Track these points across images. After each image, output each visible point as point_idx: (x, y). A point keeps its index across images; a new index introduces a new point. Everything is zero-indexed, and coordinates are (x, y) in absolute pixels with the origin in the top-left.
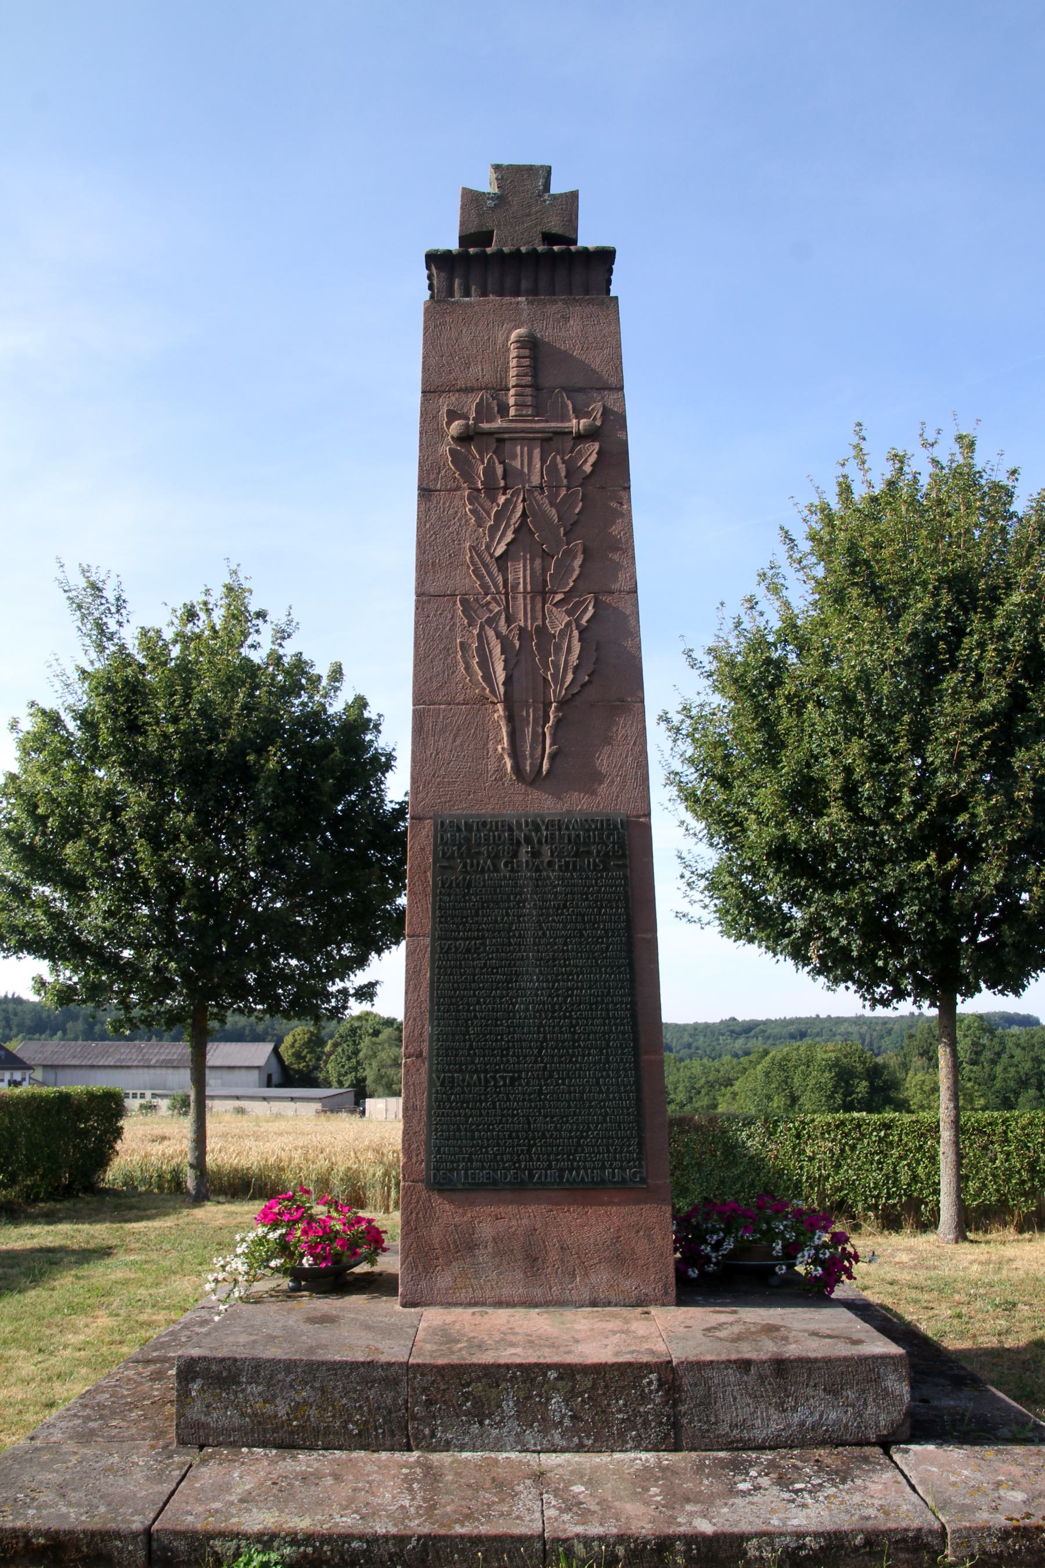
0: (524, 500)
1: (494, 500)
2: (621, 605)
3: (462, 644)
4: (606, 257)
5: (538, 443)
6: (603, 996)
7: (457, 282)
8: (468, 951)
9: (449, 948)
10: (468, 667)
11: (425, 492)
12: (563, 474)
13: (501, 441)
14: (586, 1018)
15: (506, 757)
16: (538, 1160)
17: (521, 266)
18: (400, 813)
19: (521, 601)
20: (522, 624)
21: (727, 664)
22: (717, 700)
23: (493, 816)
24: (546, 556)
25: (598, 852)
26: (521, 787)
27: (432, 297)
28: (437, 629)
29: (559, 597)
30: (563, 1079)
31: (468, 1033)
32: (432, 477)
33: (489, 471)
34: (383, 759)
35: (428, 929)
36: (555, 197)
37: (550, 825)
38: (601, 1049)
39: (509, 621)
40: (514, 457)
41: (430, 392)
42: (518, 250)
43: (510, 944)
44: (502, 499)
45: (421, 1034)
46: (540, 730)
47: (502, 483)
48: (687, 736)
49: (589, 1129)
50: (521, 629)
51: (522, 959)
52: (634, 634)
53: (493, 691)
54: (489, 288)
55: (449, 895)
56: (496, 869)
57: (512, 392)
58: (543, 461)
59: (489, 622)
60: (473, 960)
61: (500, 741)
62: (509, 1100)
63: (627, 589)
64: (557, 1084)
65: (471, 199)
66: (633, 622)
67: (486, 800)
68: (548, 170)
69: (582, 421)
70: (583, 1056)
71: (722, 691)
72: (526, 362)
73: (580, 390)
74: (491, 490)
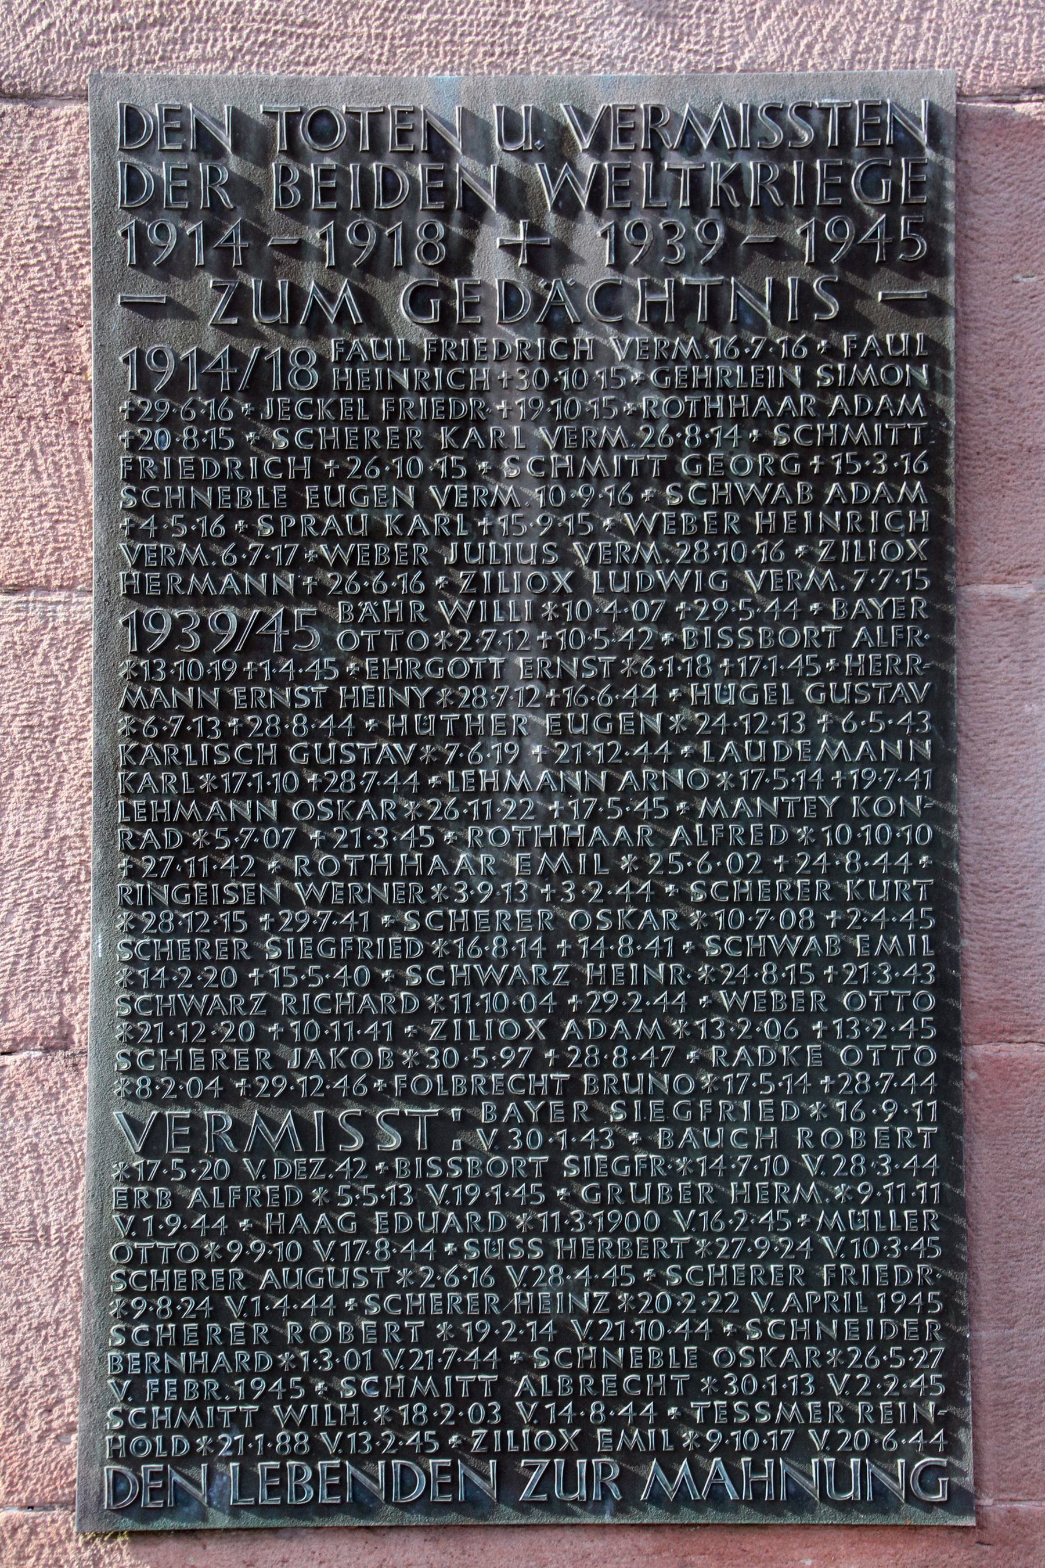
6: (820, 818)
8: (256, 645)
9: (176, 636)
14: (748, 906)
15: (459, 150)
16: (540, 1418)
23: (357, 89)
25: (824, 249)
30: (646, 1127)
31: (257, 958)
35: (85, 563)
37: (610, 130)
38: (805, 1019)
43: (435, 622)
45: (64, 966)
49: (746, 1309)
51: (486, 678)
55: (171, 421)
56: (374, 318)
60: (278, 681)
62: (423, 1202)
64: (621, 1145)
70: (731, 1043)
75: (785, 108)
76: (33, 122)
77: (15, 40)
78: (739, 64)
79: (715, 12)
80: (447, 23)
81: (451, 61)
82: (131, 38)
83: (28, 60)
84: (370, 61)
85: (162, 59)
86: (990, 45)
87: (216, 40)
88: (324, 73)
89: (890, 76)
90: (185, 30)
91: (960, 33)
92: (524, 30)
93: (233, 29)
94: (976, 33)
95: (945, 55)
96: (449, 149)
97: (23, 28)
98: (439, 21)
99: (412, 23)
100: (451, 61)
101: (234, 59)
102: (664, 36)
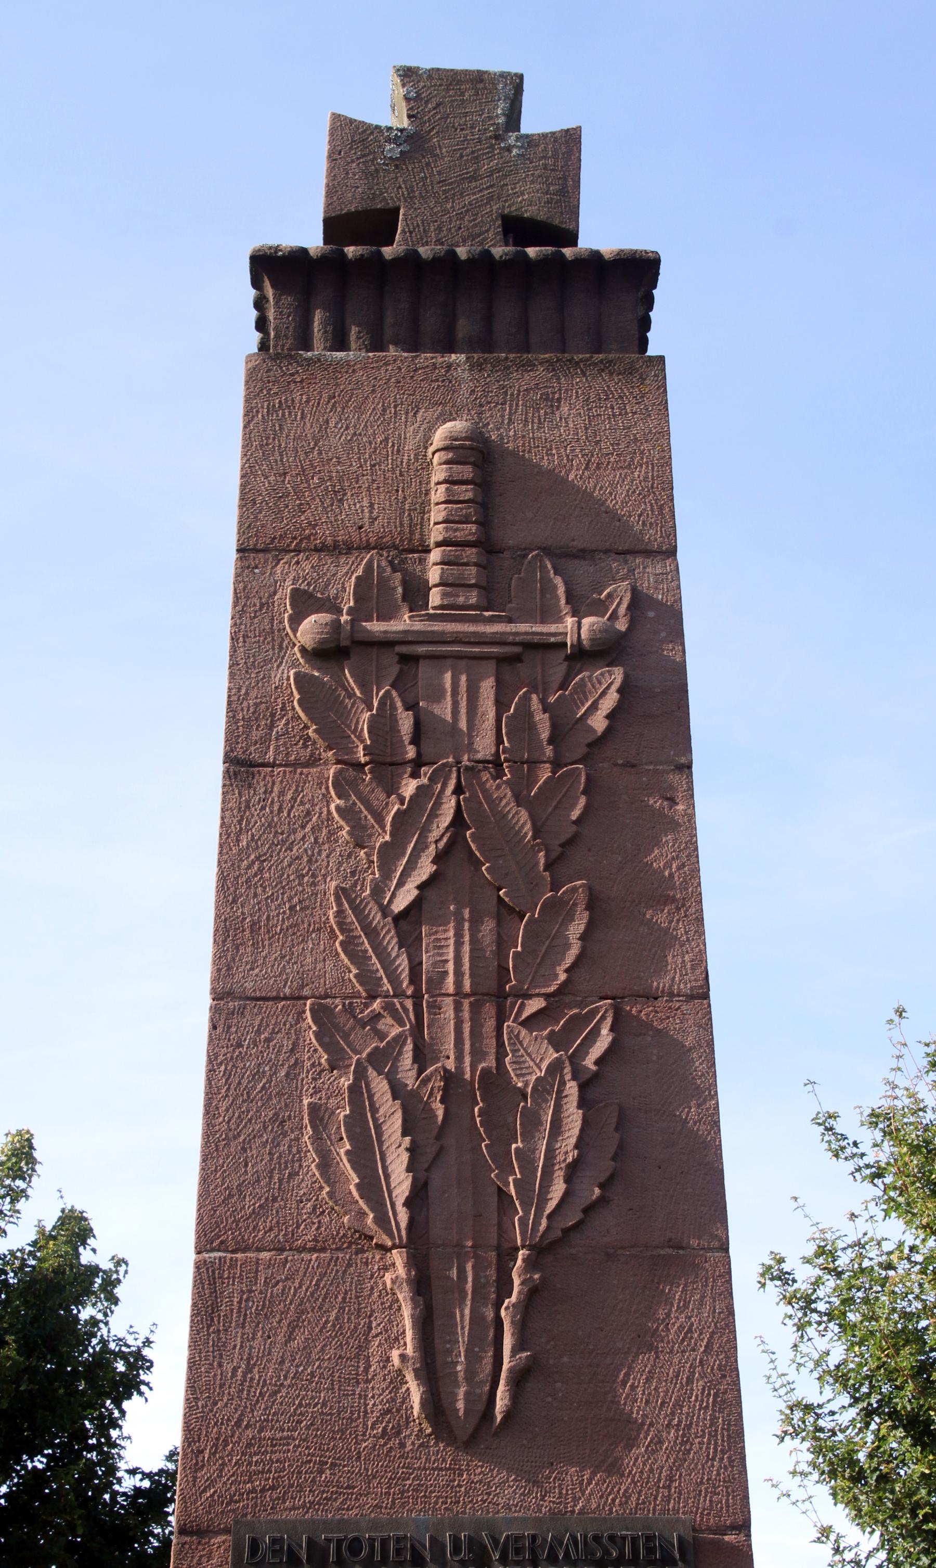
0: (458, 790)
1: (392, 789)
2: (673, 1025)
3: (313, 1108)
4: (639, 271)
5: (491, 666)
7: (318, 317)
10: (326, 1164)
11: (240, 768)
12: (545, 735)
13: (408, 660)
15: (410, 1377)
17: (453, 278)
18: (154, 1497)
19: (449, 1012)
20: (451, 1065)
21: (914, 1150)
22: (895, 1231)
23: (375, 1525)
24: (506, 913)
26: (442, 1453)
27: (263, 346)
28: (258, 1075)
29: (534, 1005)
32: (255, 735)
33: (383, 725)
34: (121, 1367)
36: (530, 141)
39: (421, 1058)
40: (437, 695)
41: (256, 549)
42: (452, 254)
44: (409, 787)
46: (490, 1314)
47: (411, 752)
48: (830, 1315)
50: (448, 1077)
52: (706, 1094)
53: (382, 1221)
54: (389, 333)
57: (435, 555)
58: (501, 705)
59: (378, 1059)
61: (397, 1340)
63: (686, 988)
65: (352, 141)
66: (700, 1065)
67: (360, 1485)
68: (516, 84)
69: (587, 621)
71: (907, 1211)
72: (466, 492)
73: (582, 554)
74: (386, 767)
75: (602, 1536)
76: (200, 1547)
77: (196, 1501)
78: (577, 1509)
79: (563, 1480)
80: (422, 1485)
81: (425, 1507)
82: (256, 1497)
83: (201, 1512)
84: (381, 1507)
85: (271, 1509)
86: (707, 1502)
87: (300, 1497)
88: (357, 1515)
89: (657, 1519)
90: (285, 1492)
91: (692, 1495)
92: (463, 1489)
93: (310, 1491)
94: (700, 1495)
95: (685, 1507)
96: (423, 1559)
97: (200, 1494)
98: (418, 1485)
99: (405, 1485)
100: (425, 1507)
101: (310, 1508)
102: (537, 1493)
